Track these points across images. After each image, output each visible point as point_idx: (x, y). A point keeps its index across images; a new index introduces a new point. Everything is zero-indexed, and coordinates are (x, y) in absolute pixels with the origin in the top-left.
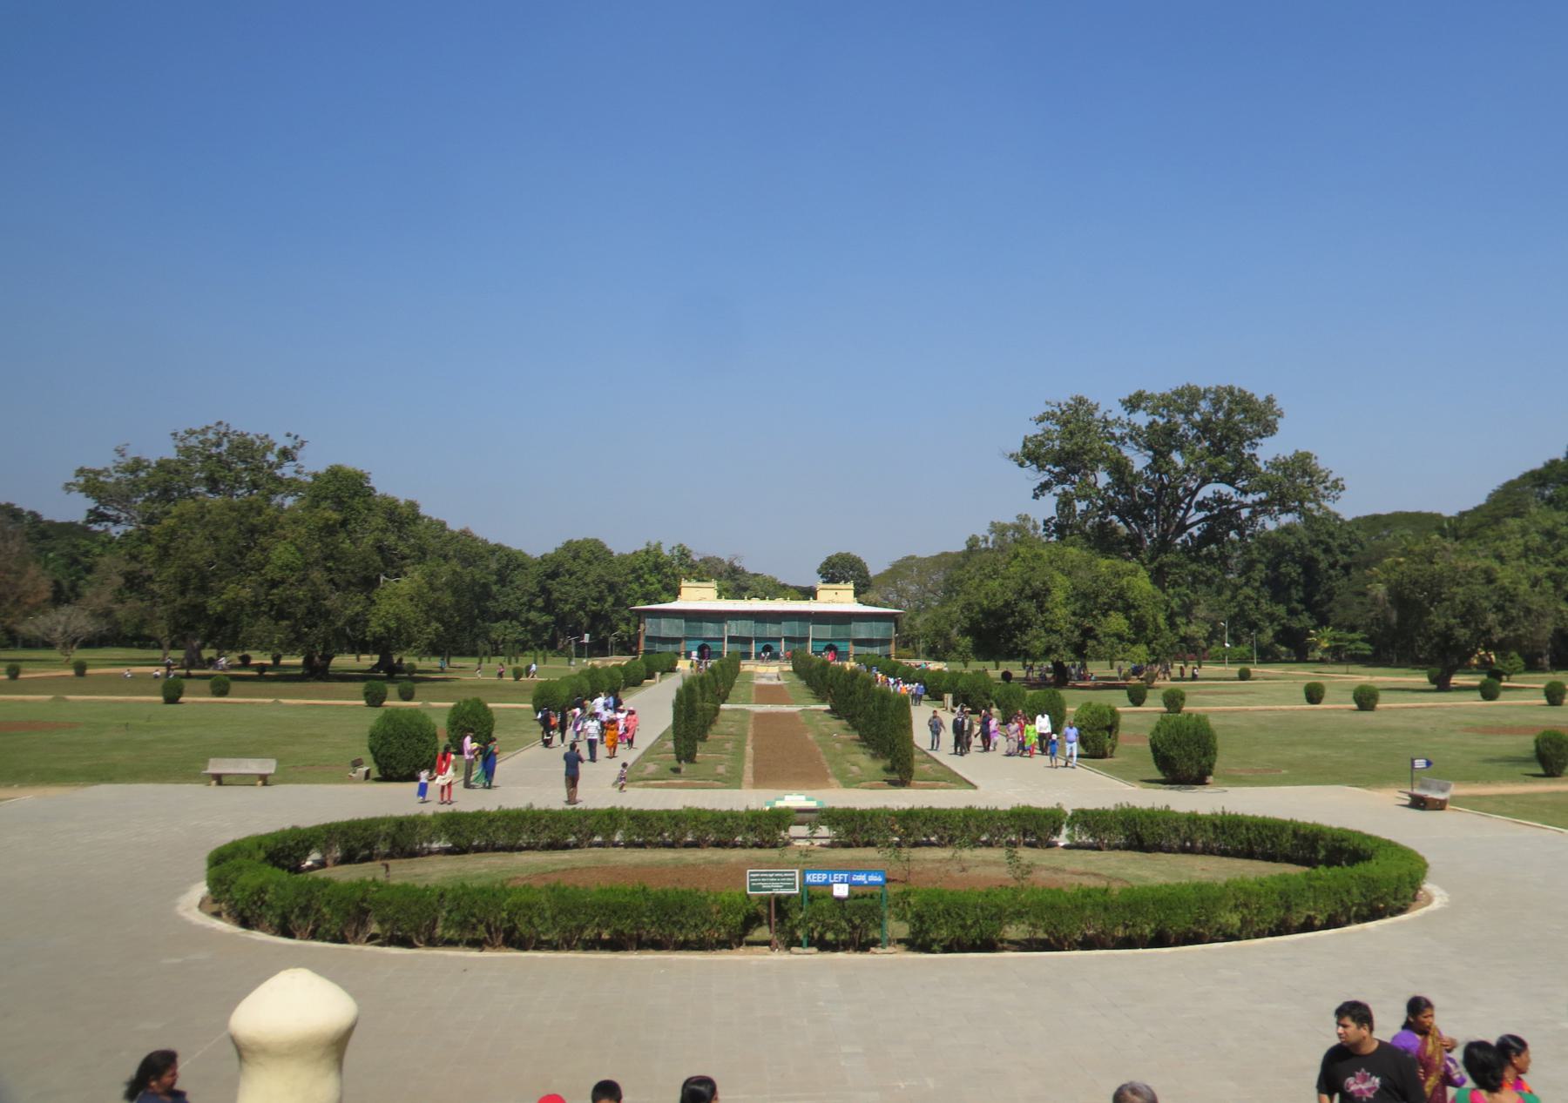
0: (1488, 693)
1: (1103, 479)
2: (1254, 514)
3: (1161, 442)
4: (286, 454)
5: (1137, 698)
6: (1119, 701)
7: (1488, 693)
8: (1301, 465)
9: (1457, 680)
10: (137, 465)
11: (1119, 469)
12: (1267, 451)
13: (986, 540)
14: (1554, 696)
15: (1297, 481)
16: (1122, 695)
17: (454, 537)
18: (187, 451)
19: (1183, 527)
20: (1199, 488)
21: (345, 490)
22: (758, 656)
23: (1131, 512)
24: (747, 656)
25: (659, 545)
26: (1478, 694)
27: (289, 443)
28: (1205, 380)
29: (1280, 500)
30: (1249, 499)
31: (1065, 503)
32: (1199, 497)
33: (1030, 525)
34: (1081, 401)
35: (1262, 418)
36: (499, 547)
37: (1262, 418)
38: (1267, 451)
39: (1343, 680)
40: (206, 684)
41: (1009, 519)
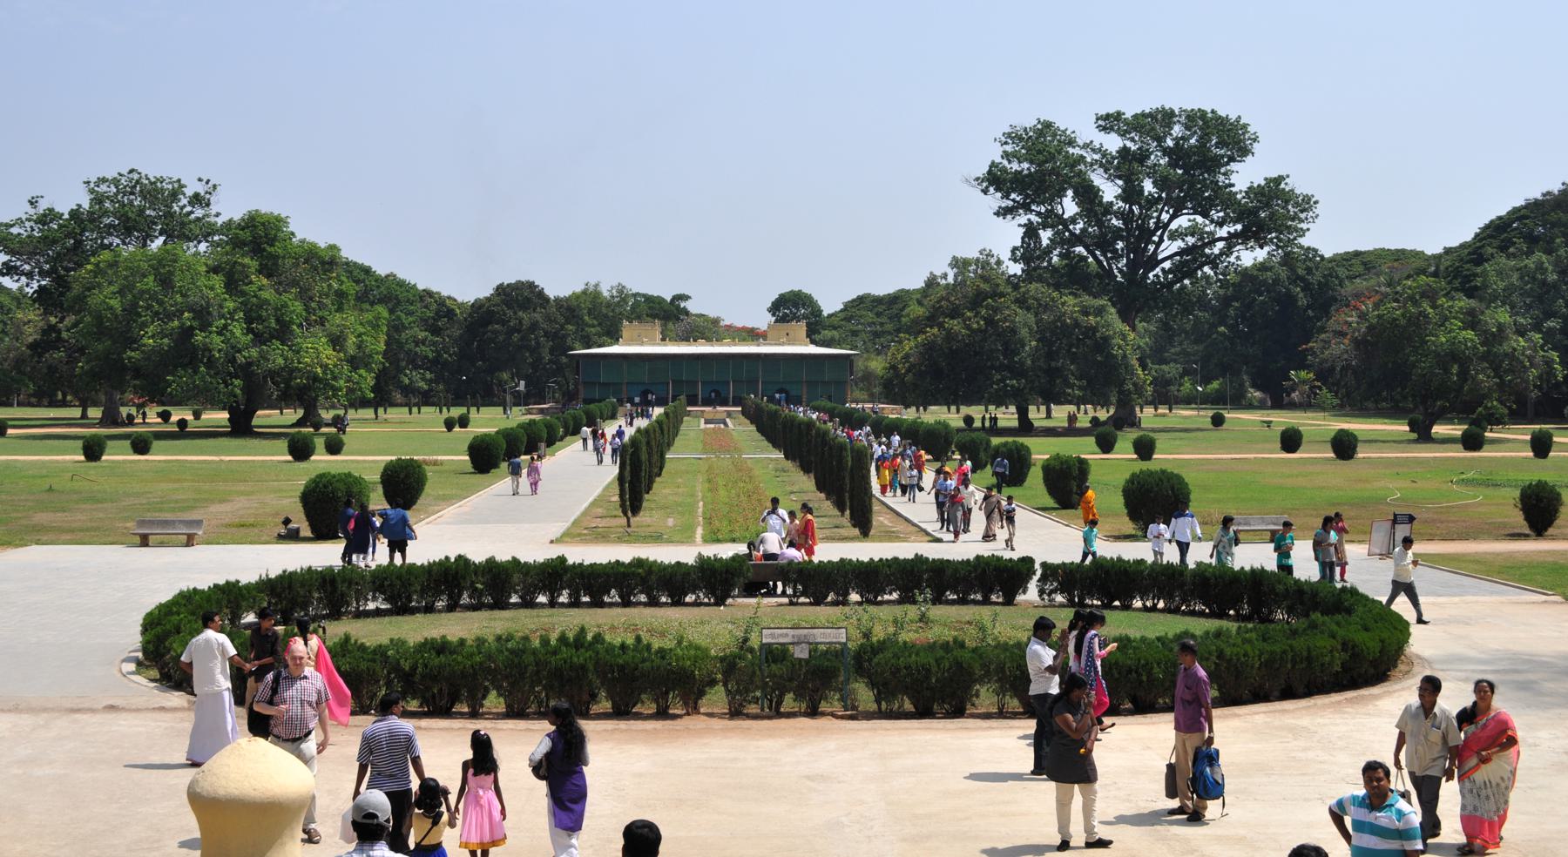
0: (1472, 442)
1: (1069, 206)
2: (1228, 251)
3: (1126, 166)
4: (197, 199)
5: (1106, 445)
6: (1085, 447)
7: (1472, 442)
8: (1272, 193)
9: (1439, 430)
10: (48, 217)
11: (1088, 195)
12: (1244, 176)
13: (945, 276)
14: (1541, 446)
15: (1271, 211)
16: (1091, 441)
17: (381, 281)
18: (98, 199)
19: (1154, 262)
20: (1170, 220)
21: (259, 237)
23: (1104, 243)
26: (1460, 446)
27: (201, 189)
28: (1181, 100)
29: (1254, 232)
30: (1223, 232)
31: (1031, 232)
32: (1173, 226)
33: (993, 261)
34: (1048, 125)
35: (1232, 139)
36: (429, 293)
37: (1232, 139)
38: (1244, 176)
39: (1319, 425)
40: (127, 443)
41: (972, 253)
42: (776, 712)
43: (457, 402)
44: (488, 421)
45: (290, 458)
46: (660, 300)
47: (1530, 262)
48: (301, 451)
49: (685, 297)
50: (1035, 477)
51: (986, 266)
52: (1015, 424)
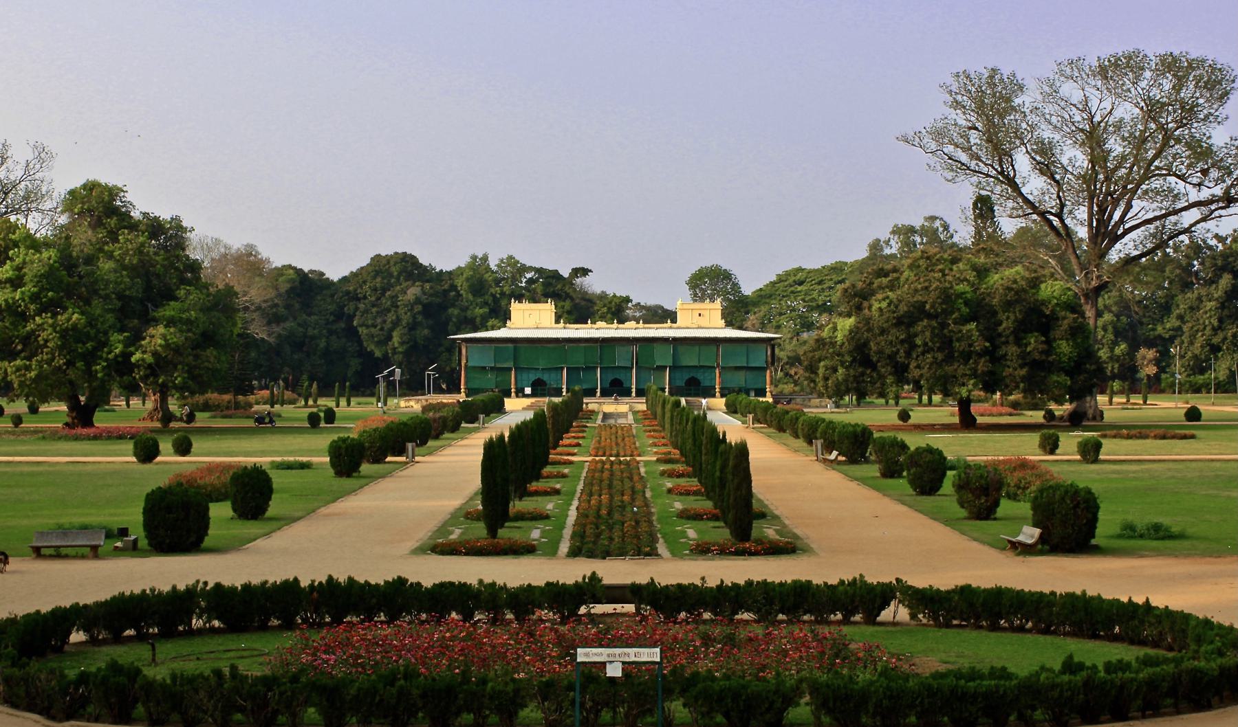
22: (605, 393)
24: (591, 393)
25: (485, 258)
42: (1178, 712)
43: (325, 391)
44: (360, 414)
45: (134, 459)
46: (555, 275)
47: (899, 292)
48: (147, 452)
49: (585, 272)
50: (948, 486)
51: (933, 232)
52: (956, 420)
